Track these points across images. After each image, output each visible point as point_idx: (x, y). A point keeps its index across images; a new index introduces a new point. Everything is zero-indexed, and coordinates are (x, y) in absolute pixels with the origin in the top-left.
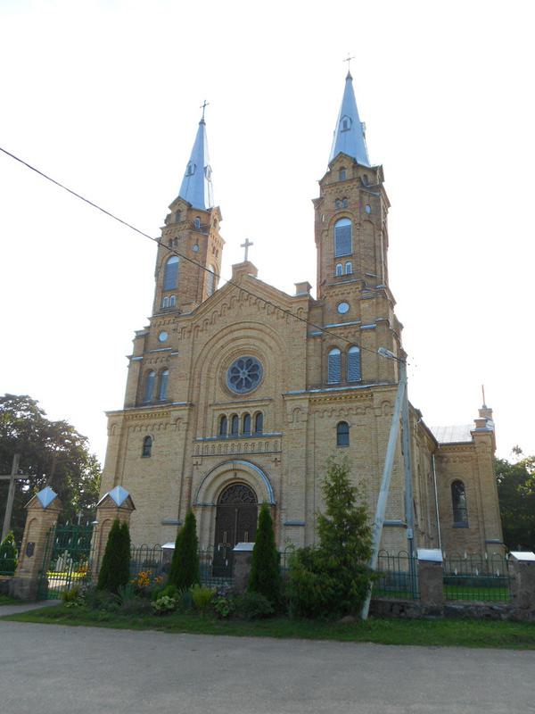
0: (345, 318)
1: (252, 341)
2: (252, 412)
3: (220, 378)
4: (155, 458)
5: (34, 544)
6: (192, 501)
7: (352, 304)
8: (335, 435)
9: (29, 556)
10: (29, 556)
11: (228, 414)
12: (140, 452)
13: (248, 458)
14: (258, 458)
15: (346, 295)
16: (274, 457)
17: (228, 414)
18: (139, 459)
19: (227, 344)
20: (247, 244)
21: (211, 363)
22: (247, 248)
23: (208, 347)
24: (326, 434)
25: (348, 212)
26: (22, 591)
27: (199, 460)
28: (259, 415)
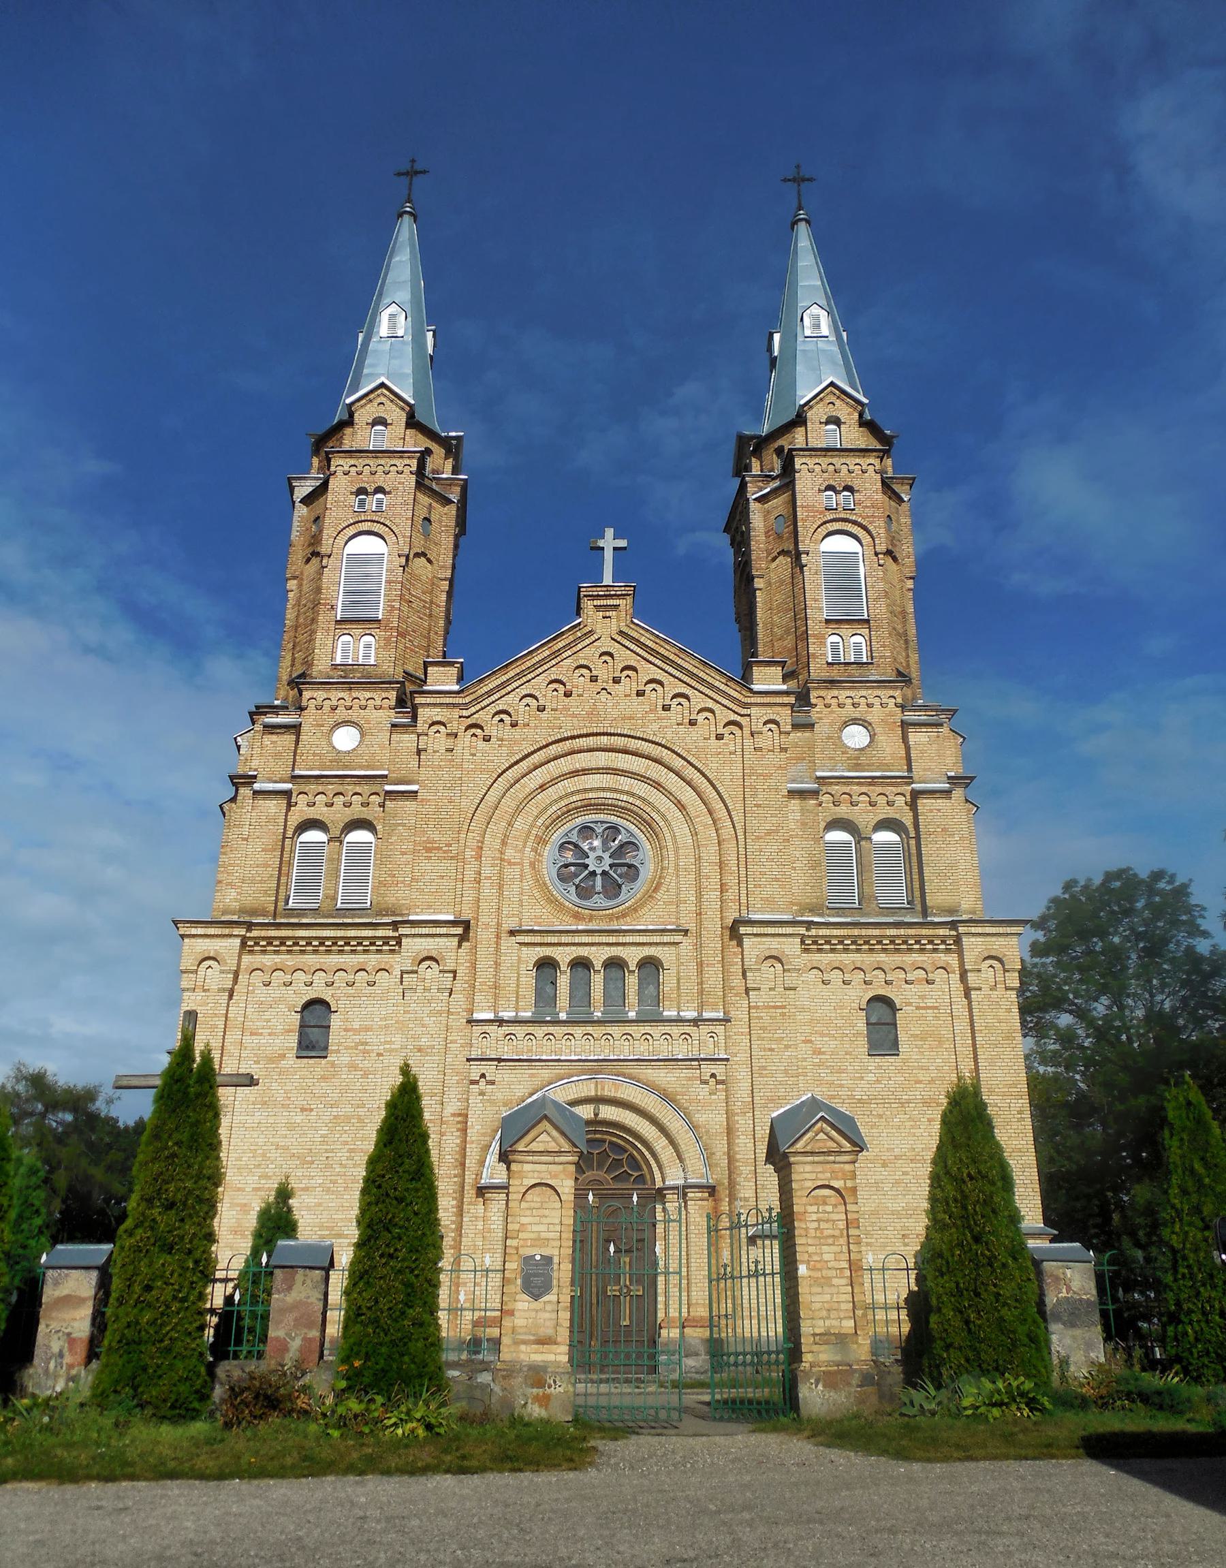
0: (863, 760)
1: (625, 783)
2: (632, 956)
3: (532, 865)
4: (345, 1059)
5: (548, 1260)
7: (878, 730)
8: (861, 1026)
9: (536, 1297)
10: (536, 1297)
11: (564, 956)
12: (293, 1041)
14: (662, 1073)
15: (863, 708)
16: (708, 1069)
17: (564, 956)
18: (291, 1061)
19: (554, 781)
21: (510, 824)
22: (794, 180)
23: (502, 782)
24: (840, 1022)
25: (855, 523)
26: (544, 1401)
27: (489, 1069)
28: (650, 965)
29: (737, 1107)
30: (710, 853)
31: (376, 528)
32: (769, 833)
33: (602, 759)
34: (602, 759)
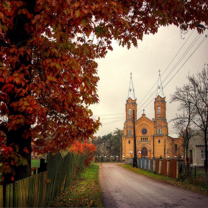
11: (142, 138)
17: (142, 138)
28: (147, 138)
33: (144, 125)
34: (144, 125)
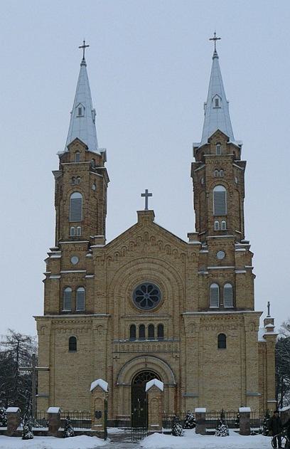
6: (114, 383)
13: (156, 355)
16: (175, 354)
20: (147, 195)
29: (182, 364)
30: (176, 293)
31: (79, 190)
32: (192, 287)
